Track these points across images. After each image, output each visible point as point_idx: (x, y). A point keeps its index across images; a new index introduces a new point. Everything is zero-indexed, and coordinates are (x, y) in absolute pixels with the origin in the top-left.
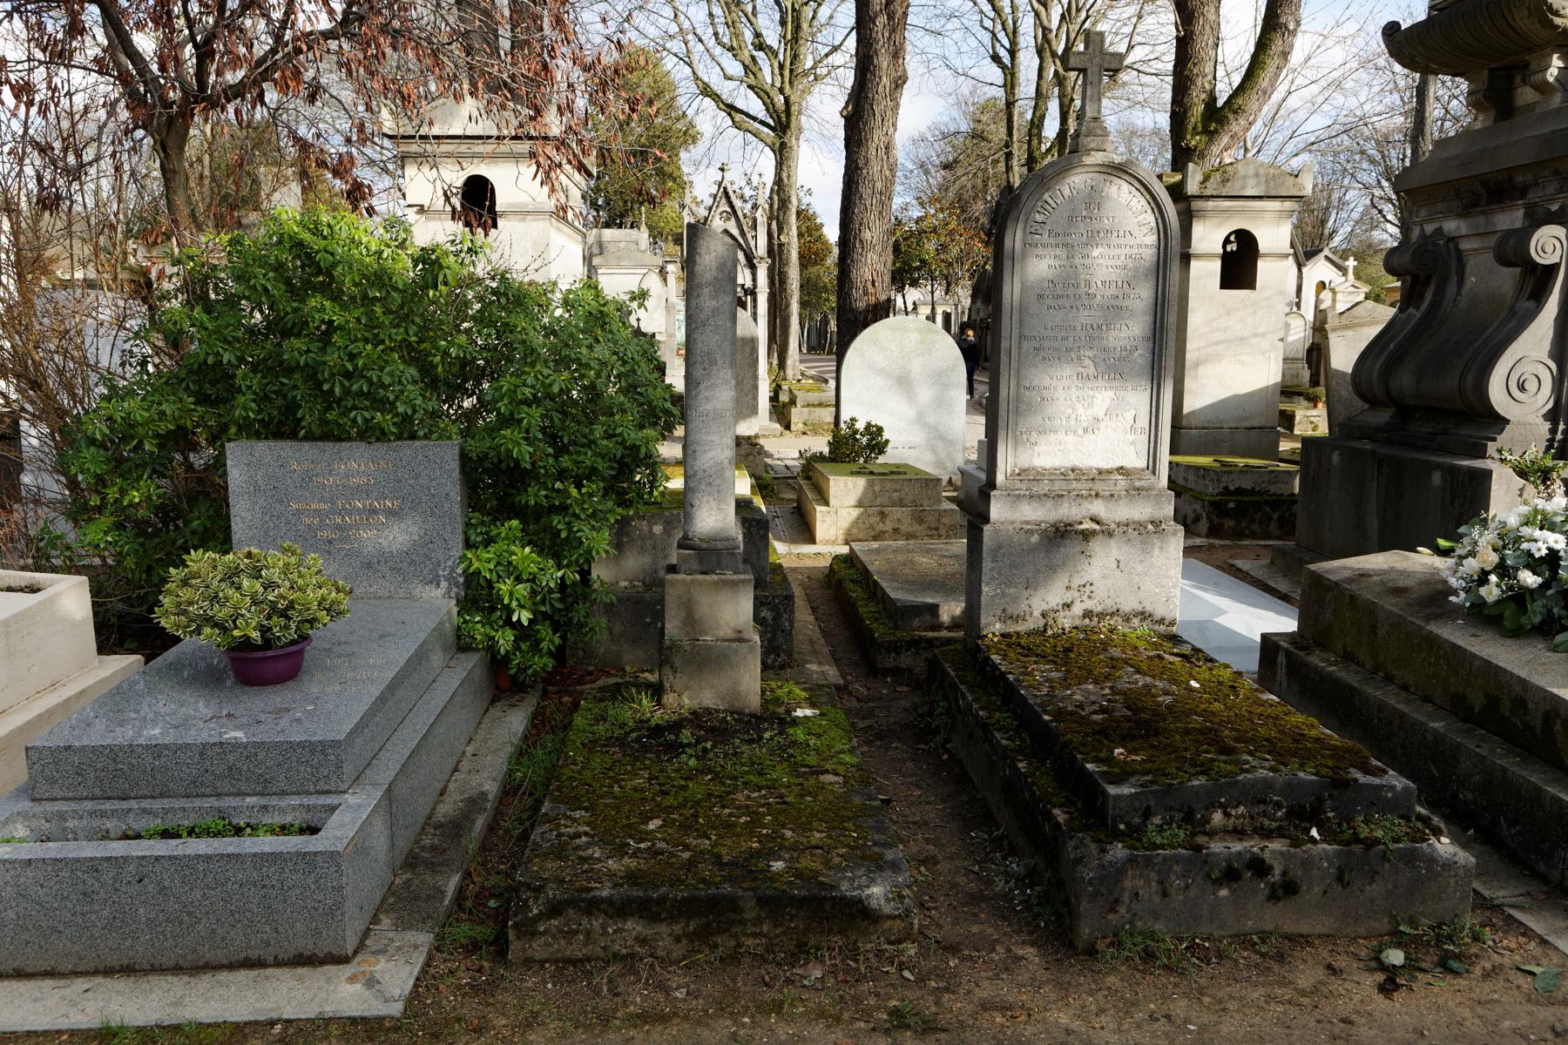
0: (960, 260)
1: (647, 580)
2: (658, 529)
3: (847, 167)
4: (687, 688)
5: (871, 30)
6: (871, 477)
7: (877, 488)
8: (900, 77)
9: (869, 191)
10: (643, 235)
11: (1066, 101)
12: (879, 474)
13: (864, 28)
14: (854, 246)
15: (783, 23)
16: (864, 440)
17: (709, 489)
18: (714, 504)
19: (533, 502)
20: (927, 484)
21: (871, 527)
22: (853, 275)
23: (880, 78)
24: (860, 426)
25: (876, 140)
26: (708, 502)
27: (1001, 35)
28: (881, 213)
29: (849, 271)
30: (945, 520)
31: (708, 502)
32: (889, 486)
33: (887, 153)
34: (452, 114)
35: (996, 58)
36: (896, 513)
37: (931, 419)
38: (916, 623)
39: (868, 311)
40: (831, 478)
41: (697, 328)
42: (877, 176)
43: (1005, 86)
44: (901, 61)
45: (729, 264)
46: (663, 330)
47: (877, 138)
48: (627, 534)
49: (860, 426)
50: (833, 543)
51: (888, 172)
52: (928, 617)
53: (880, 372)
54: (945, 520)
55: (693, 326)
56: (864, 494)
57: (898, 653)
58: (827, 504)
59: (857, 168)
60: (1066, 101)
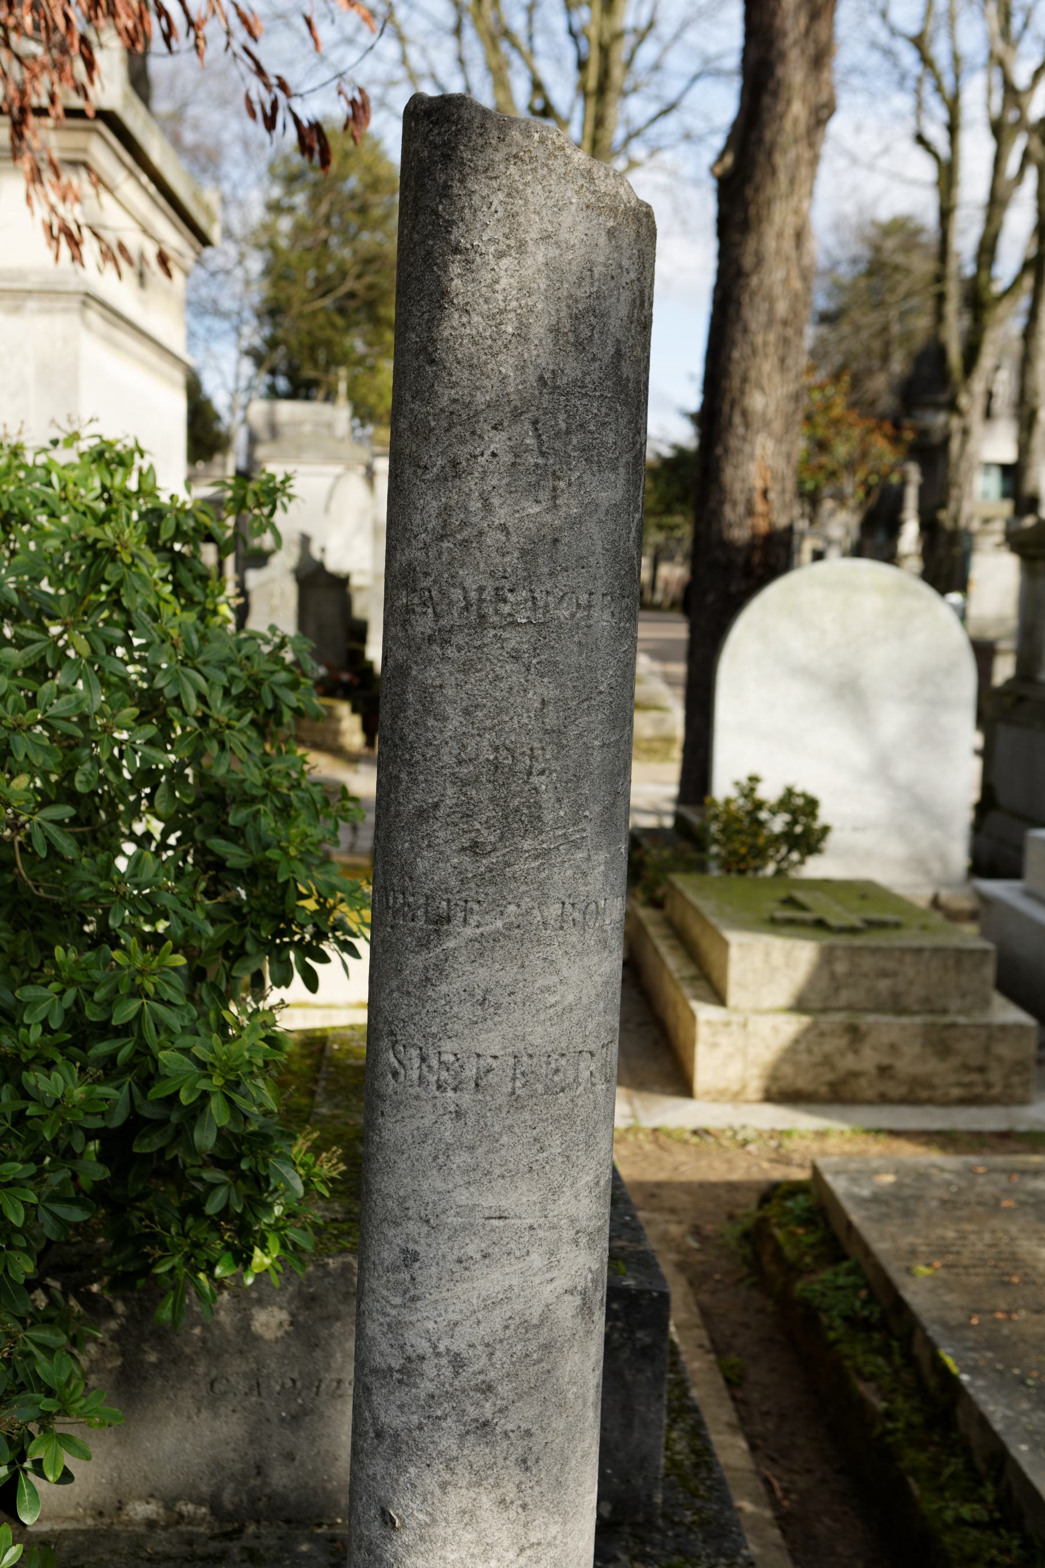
0: (850, 466)
9: (763, 318)
10: (341, 414)
15: (582, 65)
16: (778, 824)
17: (477, 1453)
20: (958, 962)
21: (827, 1061)
22: (729, 474)
24: (769, 792)
26: (469, 1515)
31: (469, 1515)
32: (867, 963)
35: (920, 139)
37: (903, 771)
40: (733, 937)
41: (442, 637)
42: (778, 290)
45: (621, 309)
48: (161, 1336)
50: (736, 1097)
55: (423, 624)
56: (812, 982)
58: (719, 998)
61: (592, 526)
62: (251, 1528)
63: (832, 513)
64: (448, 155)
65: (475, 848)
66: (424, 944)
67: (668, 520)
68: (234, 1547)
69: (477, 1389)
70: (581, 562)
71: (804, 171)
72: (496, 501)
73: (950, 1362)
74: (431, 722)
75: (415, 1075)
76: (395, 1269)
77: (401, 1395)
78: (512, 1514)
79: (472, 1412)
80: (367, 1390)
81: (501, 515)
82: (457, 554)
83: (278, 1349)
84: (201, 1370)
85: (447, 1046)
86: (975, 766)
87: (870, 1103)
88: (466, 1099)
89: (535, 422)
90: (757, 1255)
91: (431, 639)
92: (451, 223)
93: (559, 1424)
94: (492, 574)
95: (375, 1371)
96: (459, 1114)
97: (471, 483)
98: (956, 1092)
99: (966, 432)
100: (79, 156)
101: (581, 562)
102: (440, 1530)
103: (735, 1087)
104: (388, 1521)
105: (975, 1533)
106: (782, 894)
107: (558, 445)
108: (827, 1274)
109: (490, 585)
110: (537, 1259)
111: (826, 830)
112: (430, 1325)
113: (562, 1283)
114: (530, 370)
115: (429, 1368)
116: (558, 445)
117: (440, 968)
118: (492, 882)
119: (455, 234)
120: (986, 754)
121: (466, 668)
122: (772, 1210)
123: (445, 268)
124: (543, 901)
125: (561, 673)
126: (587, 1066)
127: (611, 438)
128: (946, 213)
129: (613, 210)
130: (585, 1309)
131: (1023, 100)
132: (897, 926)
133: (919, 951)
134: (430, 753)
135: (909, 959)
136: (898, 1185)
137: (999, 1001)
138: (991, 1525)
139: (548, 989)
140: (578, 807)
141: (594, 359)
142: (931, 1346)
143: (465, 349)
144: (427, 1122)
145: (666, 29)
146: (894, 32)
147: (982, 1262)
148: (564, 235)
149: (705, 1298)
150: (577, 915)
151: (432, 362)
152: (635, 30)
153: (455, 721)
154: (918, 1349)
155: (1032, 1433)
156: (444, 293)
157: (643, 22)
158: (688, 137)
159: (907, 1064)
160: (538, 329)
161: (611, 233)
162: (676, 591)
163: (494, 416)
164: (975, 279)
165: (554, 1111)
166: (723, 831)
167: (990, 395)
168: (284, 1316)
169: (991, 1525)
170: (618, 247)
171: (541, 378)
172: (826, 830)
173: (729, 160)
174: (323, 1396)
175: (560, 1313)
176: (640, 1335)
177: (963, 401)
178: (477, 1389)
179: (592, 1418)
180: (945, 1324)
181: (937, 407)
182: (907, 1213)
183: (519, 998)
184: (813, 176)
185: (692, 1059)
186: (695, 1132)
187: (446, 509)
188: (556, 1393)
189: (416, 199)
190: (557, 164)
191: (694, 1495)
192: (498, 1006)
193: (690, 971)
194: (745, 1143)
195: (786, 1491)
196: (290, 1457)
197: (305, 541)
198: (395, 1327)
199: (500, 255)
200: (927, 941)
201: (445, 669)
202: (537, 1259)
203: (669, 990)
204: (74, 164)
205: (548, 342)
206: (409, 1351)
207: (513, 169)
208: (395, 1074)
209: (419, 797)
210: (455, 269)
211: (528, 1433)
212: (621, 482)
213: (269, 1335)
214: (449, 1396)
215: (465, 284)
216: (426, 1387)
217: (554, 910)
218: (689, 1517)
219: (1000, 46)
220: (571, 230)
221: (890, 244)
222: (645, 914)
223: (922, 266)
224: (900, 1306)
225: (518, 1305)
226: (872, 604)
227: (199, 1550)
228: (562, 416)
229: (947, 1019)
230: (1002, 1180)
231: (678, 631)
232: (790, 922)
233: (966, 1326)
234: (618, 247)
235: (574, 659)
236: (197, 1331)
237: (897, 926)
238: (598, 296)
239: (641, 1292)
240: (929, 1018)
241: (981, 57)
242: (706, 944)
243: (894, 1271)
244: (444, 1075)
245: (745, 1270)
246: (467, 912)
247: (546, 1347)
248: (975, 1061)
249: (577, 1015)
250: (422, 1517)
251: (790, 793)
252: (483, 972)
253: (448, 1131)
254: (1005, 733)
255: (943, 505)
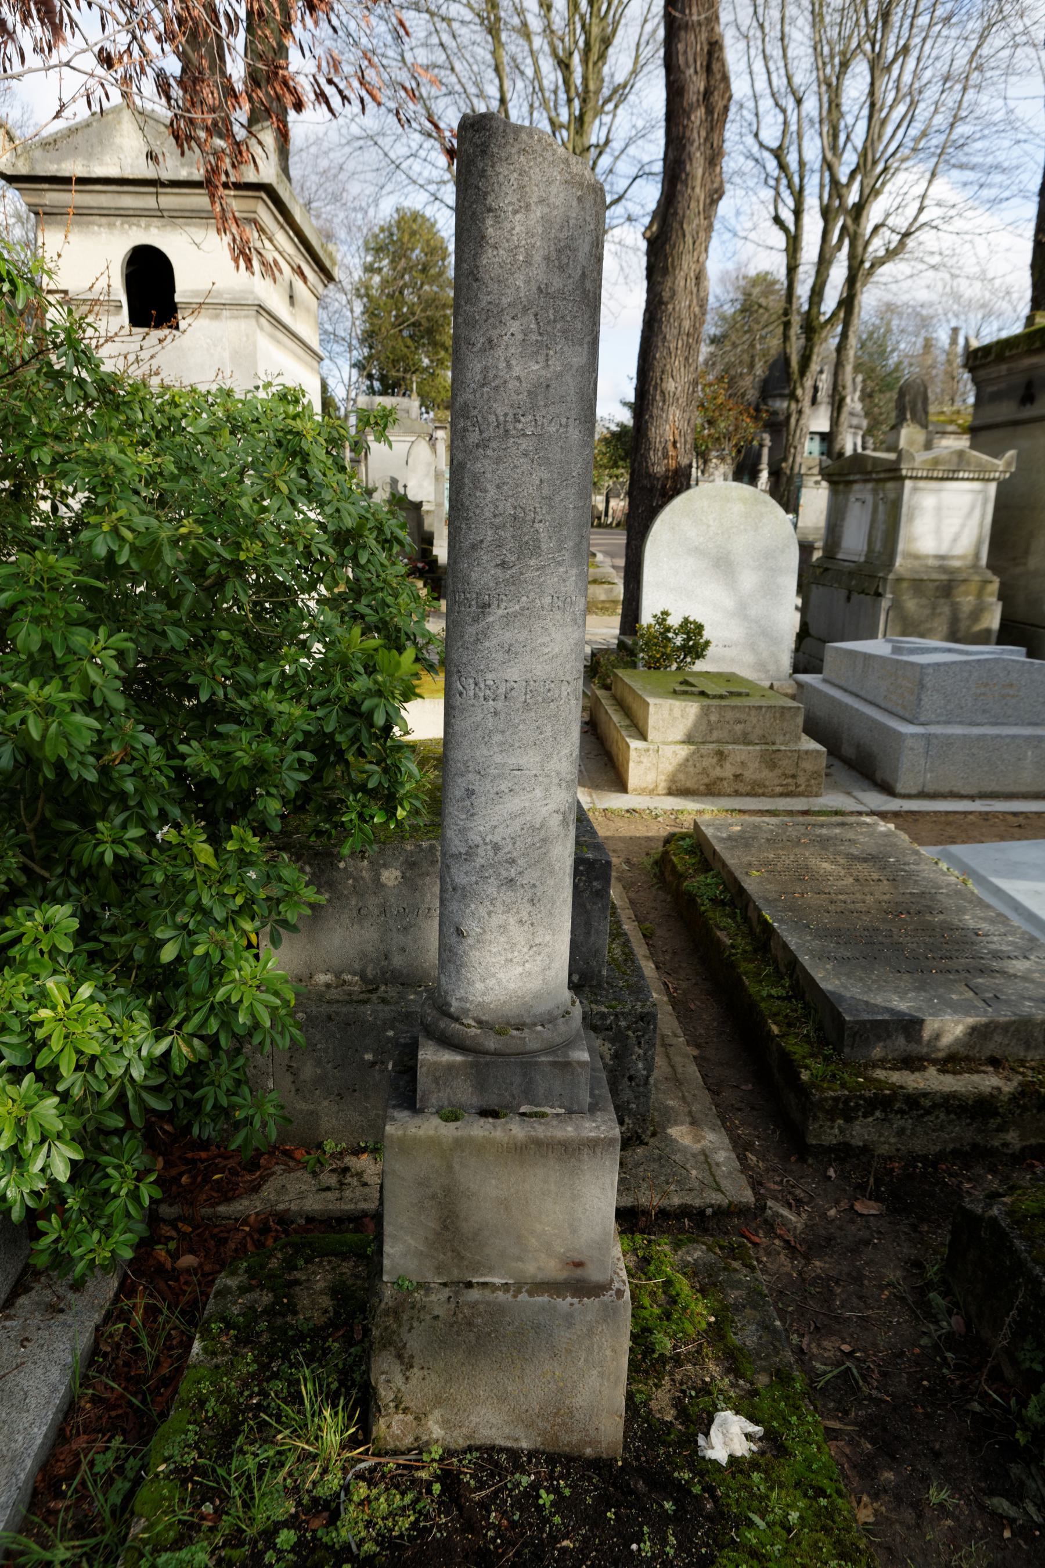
1: (370, 973)
2: (390, 876)
3: (648, 302)
4: (438, 1401)
5: (685, 127)
6: (707, 702)
7: (713, 718)
8: (716, 191)
11: (856, 263)
12: (715, 697)
13: (677, 125)
14: (654, 399)
16: (679, 641)
17: (507, 896)
18: (519, 935)
19: (109, 858)
20: (782, 714)
21: (705, 772)
23: (693, 188)
24: (674, 621)
25: (685, 266)
27: (786, 194)
28: (687, 359)
29: (647, 429)
30: (807, 765)
31: (503, 928)
32: (729, 715)
33: (698, 284)
34: (101, 142)
35: (777, 220)
36: (739, 752)
38: (877, 1052)
39: (667, 478)
40: (651, 701)
41: (484, 444)
42: (684, 313)
43: (787, 250)
44: (718, 169)
46: (432, 498)
47: (687, 265)
49: (674, 621)
50: (652, 792)
51: (697, 309)
52: (901, 1041)
53: (698, 551)
54: (807, 765)
55: (474, 437)
56: (696, 725)
57: (849, 1120)
58: (643, 736)
59: (661, 302)
60: (856, 263)
61: (568, 378)
62: (383, 988)
63: (716, 467)
64: (484, 150)
65: (503, 565)
66: (476, 620)
67: (616, 471)
68: (374, 997)
69: (507, 861)
70: (562, 399)
71: (702, 235)
72: (514, 363)
73: (768, 917)
74: (478, 494)
75: (472, 693)
76: (462, 800)
77: (466, 867)
78: (526, 928)
79: (504, 874)
80: (448, 866)
81: (517, 371)
82: (492, 394)
83: (395, 891)
84: (353, 903)
85: (489, 676)
86: (798, 616)
87: (729, 795)
88: (500, 705)
89: (536, 315)
90: (662, 873)
91: (478, 446)
92: (486, 193)
93: (551, 882)
94: (512, 406)
95: (452, 856)
96: (496, 714)
97: (500, 352)
98: (778, 789)
99: (800, 412)
100: (252, 215)
101: (562, 399)
102: (488, 937)
103: (651, 787)
104: (459, 933)
105: (778, 1002)
106: (681, 679)
107: (549, 329)
108: (701, 878)
109: (511, 412)
110: (538, 793)
111: (707, 643)
112: (481, 828)
113: (552, 806)
114: (533, 283)
115: (481, 851)
116: (549, 329)
117: (485, 634)
118: (514, 584)
119: (490, 200)
120: (803, 610)
121: (498, 461)
122: (671, 847)
123: (483, 222)
124: (541, 594)
125: (551, 464)
126: (566, 689)
127: (579, 326)
128: (792, 269)
129: (581, 185)
130: (565, 822)
131: (844, 191)
132: (747, 695)
133: (760, 707)
134: (478, 511)
135: (753, 712)
136: (743, 831)
137: (805, 738)
138: (788, 998)
139: (544, 644)
140: (561, 542)
141: (570, 277)
142: (758, 910)
143: (496, 271)
144: (479, 719)
145: (616, 145)
146: (761, 145)
147: (789, 869)
148: (552, 200)
149: (632, 895)
150: (560, 604)
151: (477, 280)
152: (597, 146)
153: (492, 492)
154: (751, 913)
155: (811, 951)
156: (483, 237)
157: (602, 141)
158: (630, 219)
159: (751, 774)
160: (538, 258)
161: (580, 199)
162: (619, 515)
163: (512, 311)
164: (809, 312)
165: (548, 712)
166: (646, 644)
167: (816, 389)
168: (398, 873)
169: (788, 998)
170: (583, 208)
171: (539, 288)
172: (707, 643)
173: (655, 228)
174: (420, 917)
175: (551, 823)
176: (595, 884)
177: (799, 392)
178: (507, 861)
179: (568, 882)
180: (766, 899)
181: (782, 396)
182: (747, 845)
183: (528, 648)
184: (708, 238)
185: (627, 771)
186: (628, 811)
187: (486, 368)
188: (550, 865)
189: (466, 180)
190: (548, 155)
191: (624, 973)
192: (517, 653)
193: (628, 722)
194: (657, 816)
195: (676, 989)
196: (403, 950)
197: (394, 482)
198: (463, 831)
199: (515, 212)
200: (764, 703)
201: (486, 462)
202: (538, 793)
203: (614, 733)
204: (249, 221)
205: (544, 265)
206: (470, 843)
207: (522, 158)
208: (461, 694)
209: (472, 537)
210: (489, 222)
211: (534, 886)
212: (585, 353)
213: (390, 884)
214: (492, 866)
215: (495, 230)
216: (480, 861)
217: (547, 600)
218: (621, 983)
219: (829, 155)
220: (557, 196)
221: (756, 291)
222: (600, 693)
223: (776, 303)
224: (741, 891)
225: (529, 818)
226: (738, 508)
227: (355, 998)
228: (551, 311)
229: (775, 748)
230: (802, 829)
231: (620, 539)
232: (685, 693)
233: (779, 900)
234: (583, 208)
235: (558, 456)
236: (350, 881)
237: (747, 695)
238: (572, 238)
239: (596, 861)
240: (764, 747)
241: (817, 166)
242: (635, 706)
243: (739, 874)
244: (488, 692)
245: (655, 880)
246: (500, 601)
247: (544, 840)
248: (790, 771)
249: (560, 660)
250: (478, 930)
251: (686, 621)
252: (508, 634)
253: (490, 723)
254: (816, 592)
255: (785, 459)
